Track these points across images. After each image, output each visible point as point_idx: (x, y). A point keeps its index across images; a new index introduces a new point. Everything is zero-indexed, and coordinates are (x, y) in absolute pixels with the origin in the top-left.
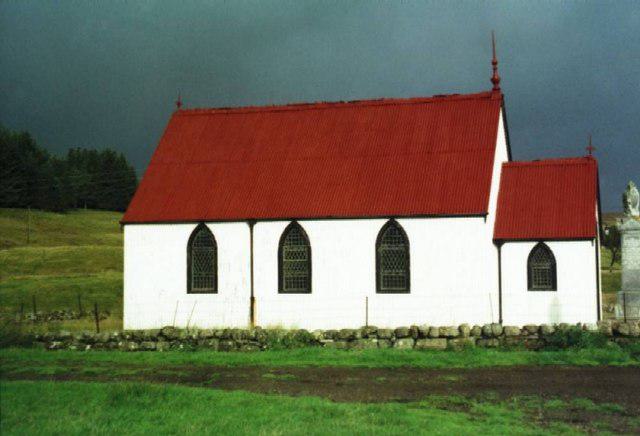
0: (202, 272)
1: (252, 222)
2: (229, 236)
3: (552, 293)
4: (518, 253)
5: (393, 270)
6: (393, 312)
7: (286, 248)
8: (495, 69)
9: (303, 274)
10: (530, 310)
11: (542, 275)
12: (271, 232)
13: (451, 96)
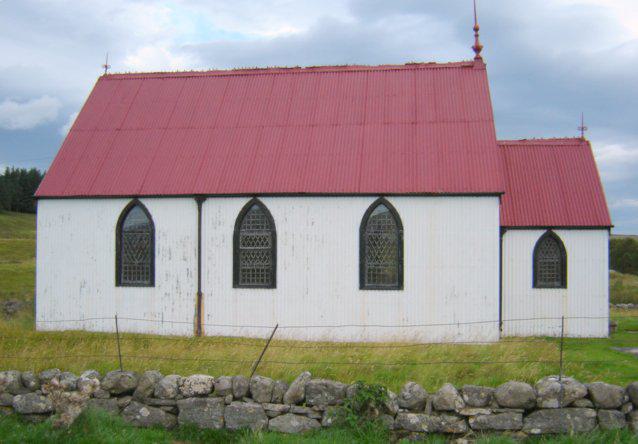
0: (135, 261)
1: (200, 199)
2: (171, 219)
3: (562, 290)
4: (524, 243)
5: (381, 261)
6: (239, 314)
7: (244, 233)
8: (477, 36)
9: (264, 265)
10: (540, 313)
11: (550, 270)
12: (224, 214)
13: (426, 65)
